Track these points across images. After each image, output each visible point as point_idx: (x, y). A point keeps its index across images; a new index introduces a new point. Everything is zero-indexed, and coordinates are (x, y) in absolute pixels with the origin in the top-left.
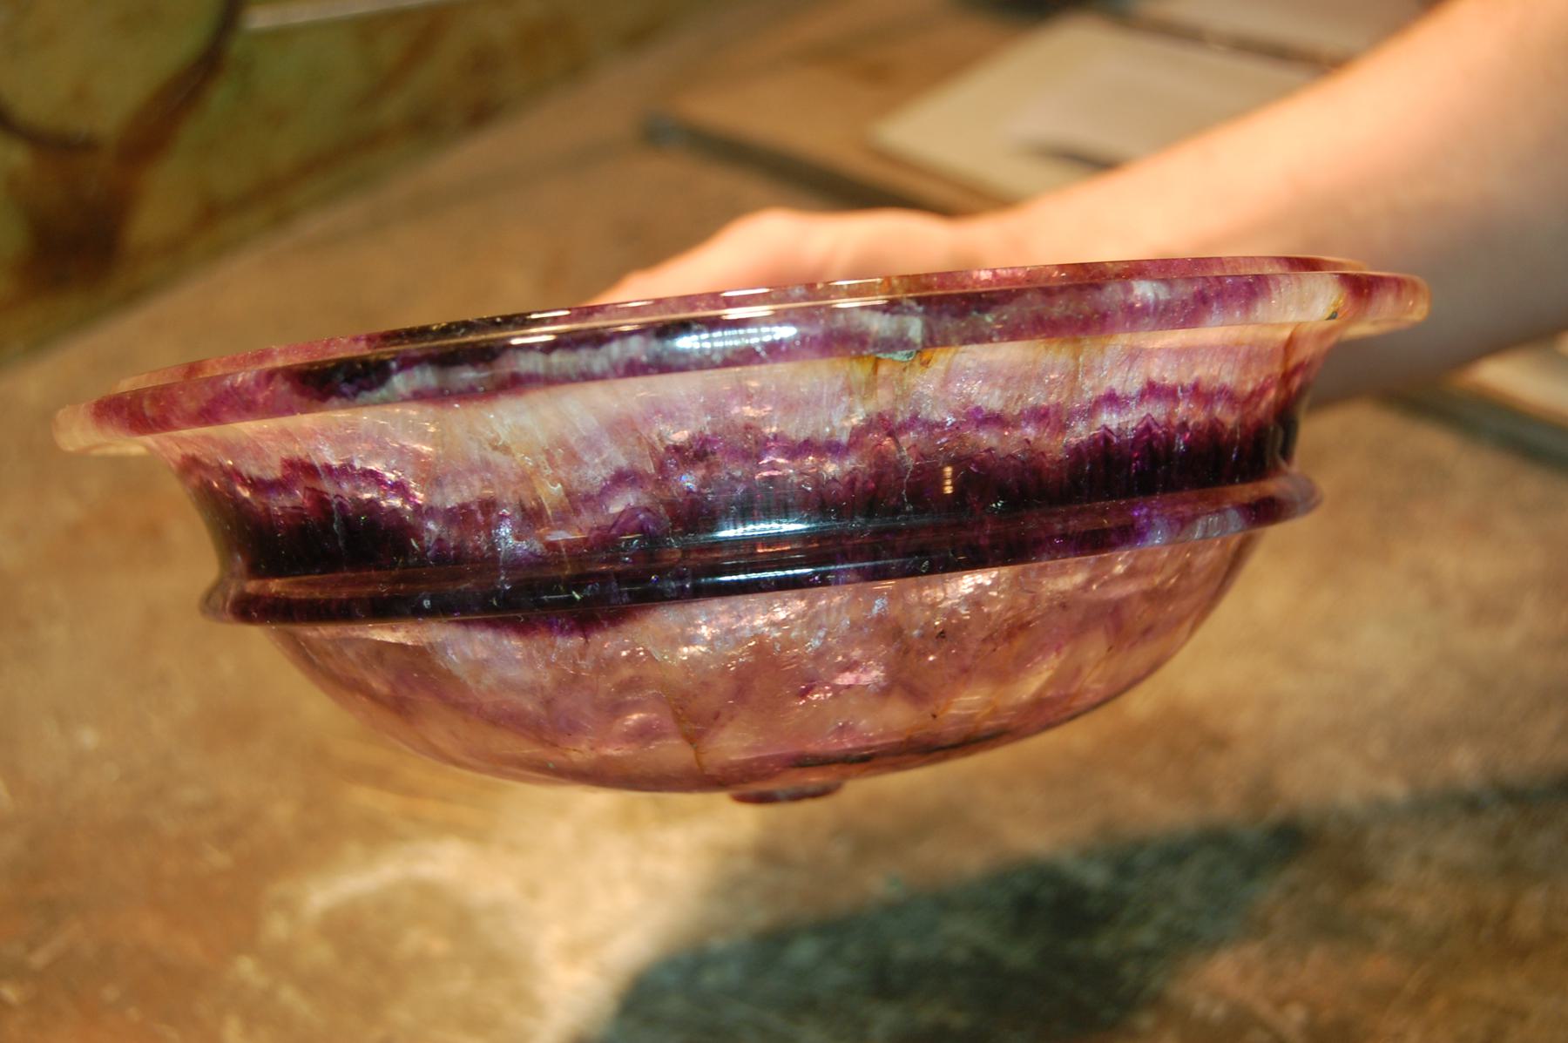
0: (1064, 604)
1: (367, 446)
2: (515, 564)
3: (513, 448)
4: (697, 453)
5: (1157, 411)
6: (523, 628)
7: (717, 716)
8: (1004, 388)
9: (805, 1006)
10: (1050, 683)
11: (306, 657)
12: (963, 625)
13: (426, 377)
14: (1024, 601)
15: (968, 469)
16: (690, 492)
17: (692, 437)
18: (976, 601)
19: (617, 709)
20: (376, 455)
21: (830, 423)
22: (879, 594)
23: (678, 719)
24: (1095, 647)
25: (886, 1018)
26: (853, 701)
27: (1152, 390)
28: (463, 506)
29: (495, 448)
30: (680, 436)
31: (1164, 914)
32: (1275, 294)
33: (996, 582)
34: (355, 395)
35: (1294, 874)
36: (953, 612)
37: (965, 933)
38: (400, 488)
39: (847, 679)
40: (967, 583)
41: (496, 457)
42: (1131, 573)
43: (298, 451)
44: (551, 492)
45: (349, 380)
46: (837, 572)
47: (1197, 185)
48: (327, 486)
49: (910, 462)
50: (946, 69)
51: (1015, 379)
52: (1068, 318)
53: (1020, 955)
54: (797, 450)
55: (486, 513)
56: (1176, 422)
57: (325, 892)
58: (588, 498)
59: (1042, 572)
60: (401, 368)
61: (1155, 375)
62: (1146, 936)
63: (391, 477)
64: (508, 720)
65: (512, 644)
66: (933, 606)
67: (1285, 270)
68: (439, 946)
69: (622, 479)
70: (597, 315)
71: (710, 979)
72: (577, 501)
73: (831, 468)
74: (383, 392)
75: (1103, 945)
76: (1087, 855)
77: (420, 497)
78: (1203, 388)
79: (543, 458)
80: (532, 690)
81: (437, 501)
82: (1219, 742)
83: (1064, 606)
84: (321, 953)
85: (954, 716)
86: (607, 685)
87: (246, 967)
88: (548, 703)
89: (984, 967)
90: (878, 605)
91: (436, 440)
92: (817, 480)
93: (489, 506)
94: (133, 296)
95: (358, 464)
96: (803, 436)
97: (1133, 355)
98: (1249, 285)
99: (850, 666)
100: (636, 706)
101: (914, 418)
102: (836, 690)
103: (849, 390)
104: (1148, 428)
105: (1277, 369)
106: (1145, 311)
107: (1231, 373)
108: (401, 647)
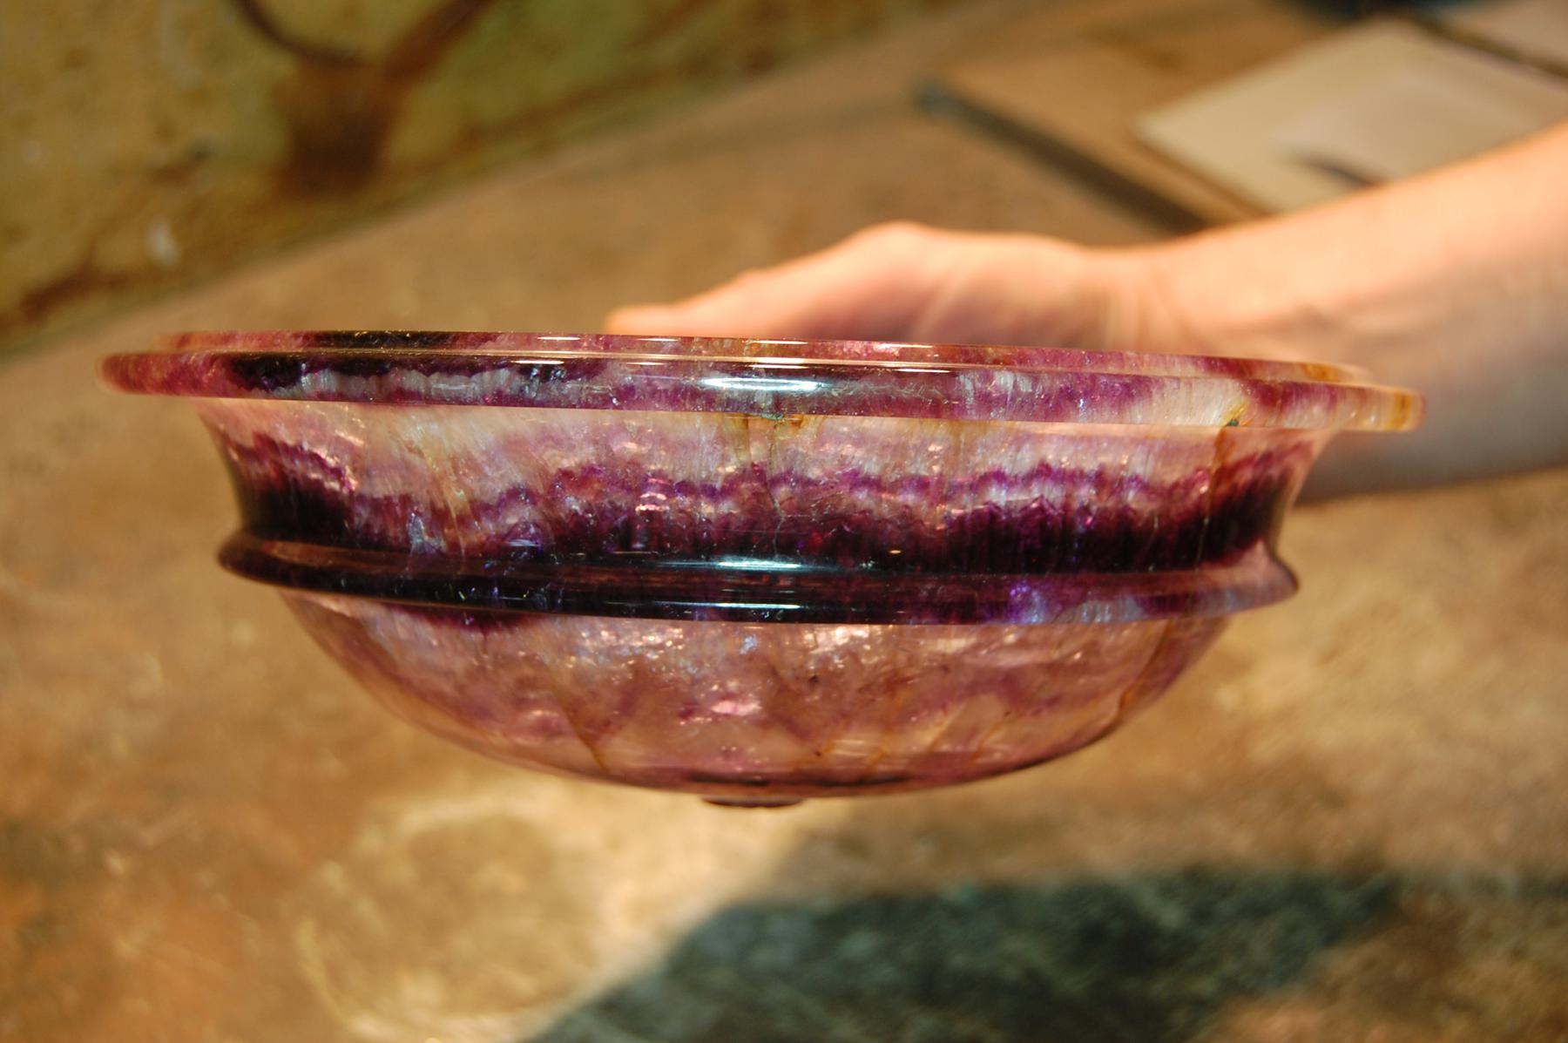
0: (947, 665)
1: (312, 433)
2: (423, 553)
3: (426, 452)
4: (579, 479)
5: (1053, 494)
6: (434, 617)
7: (607, 724)
8: (881, 456)
9: (846, 998)
10: (949, 734)
11: (302, 609)
12: (838, 674)
13: (326, 380)
14: (902, 657)
15: (841, 529)
16: (576, 513)
17: (580, 465)
18: (851, 652)
19: (521, 704)
20: (319, 441)
21: (707, 469)
22: (749, 633)
23: (573, 721)
24: (990, 707)
25: (923, 1022)
26: (736, 729)
27: (1044, 472)
28: (388, 499)
29: (411, 450)
30: (567, 463)
31: (1230, 966)
32: (1156, 397)
33: (870, 640)
34: (273, 388)
35: (1373, 949)
36: (825, 660)
37: (1023, 951)
38: (337, 473)
39: (724, 707)
40: (840, 634)
41: (414, 459)
42: (1022, 644)
43: (265, 427)
44: (456, 497)
45: (268, 375)
46: (694, 609)
47: (1359, 235)
48: (285, 461)
49: (783, 515)
50: (1241, 62)
51: (899, 449)
52: (918, 400)
53: (1072, 984)
54: (671, 489)
55: (404, 508)
56: (1076, 505)
57: (421, 815)
58: (486, 508)
59: (921, 634)
60: (310, 370)
61: (1050, 458)
62: (1206, 986)
63: (331, 462)
64: (429, 697)
65: (426, 631)
66: (805, 651)
67: (1201, 372)
68: (513, 882)
69: (513, 494)
70: (489, 343)
71: (763, 957)
72: (479, 509)
73: (707, 509)
74: (295, 390)
75: (1160, 988)
76: (1167, 890)
77: (354, 483)
78: (1110, 474)
79: (449, 465)
80: (448, 674)
81: (366, 490)
82: (1335, 799)
83: (945, 668)
84: (402, 872)
85: (838, 756)
86: (507, 679)
87: (333, 876)
88: (461, 688)
89: (1035, 988)
90: (750, 643)
91: (366, 436)
92: (691, 519)
93: (406, 500)
94: (389, 208)
95: (306, 447)
96: (680, 476)
97: (1019, 440)
98: (1126, 386)
99: (727, 696)
100: (535, 704)
101: (789, 472)
102: (716, 716)
103: (722, 440)
104: (1041, 509)
105: (1211, 463)
106: (1002, 401)
107: (1145, 463)
108: (340, 616)
